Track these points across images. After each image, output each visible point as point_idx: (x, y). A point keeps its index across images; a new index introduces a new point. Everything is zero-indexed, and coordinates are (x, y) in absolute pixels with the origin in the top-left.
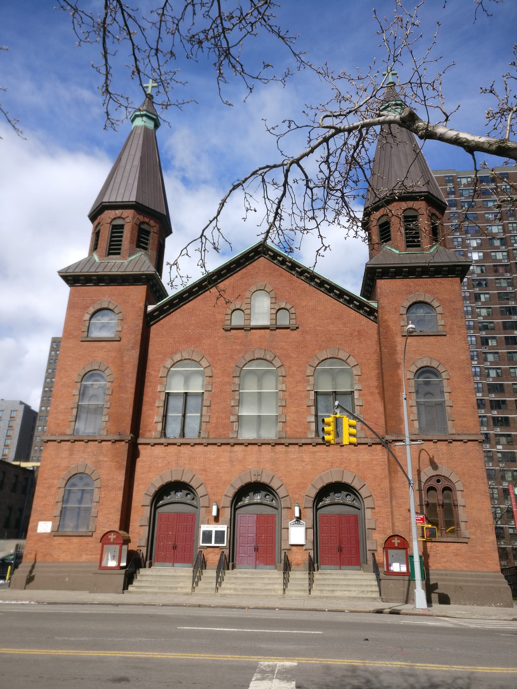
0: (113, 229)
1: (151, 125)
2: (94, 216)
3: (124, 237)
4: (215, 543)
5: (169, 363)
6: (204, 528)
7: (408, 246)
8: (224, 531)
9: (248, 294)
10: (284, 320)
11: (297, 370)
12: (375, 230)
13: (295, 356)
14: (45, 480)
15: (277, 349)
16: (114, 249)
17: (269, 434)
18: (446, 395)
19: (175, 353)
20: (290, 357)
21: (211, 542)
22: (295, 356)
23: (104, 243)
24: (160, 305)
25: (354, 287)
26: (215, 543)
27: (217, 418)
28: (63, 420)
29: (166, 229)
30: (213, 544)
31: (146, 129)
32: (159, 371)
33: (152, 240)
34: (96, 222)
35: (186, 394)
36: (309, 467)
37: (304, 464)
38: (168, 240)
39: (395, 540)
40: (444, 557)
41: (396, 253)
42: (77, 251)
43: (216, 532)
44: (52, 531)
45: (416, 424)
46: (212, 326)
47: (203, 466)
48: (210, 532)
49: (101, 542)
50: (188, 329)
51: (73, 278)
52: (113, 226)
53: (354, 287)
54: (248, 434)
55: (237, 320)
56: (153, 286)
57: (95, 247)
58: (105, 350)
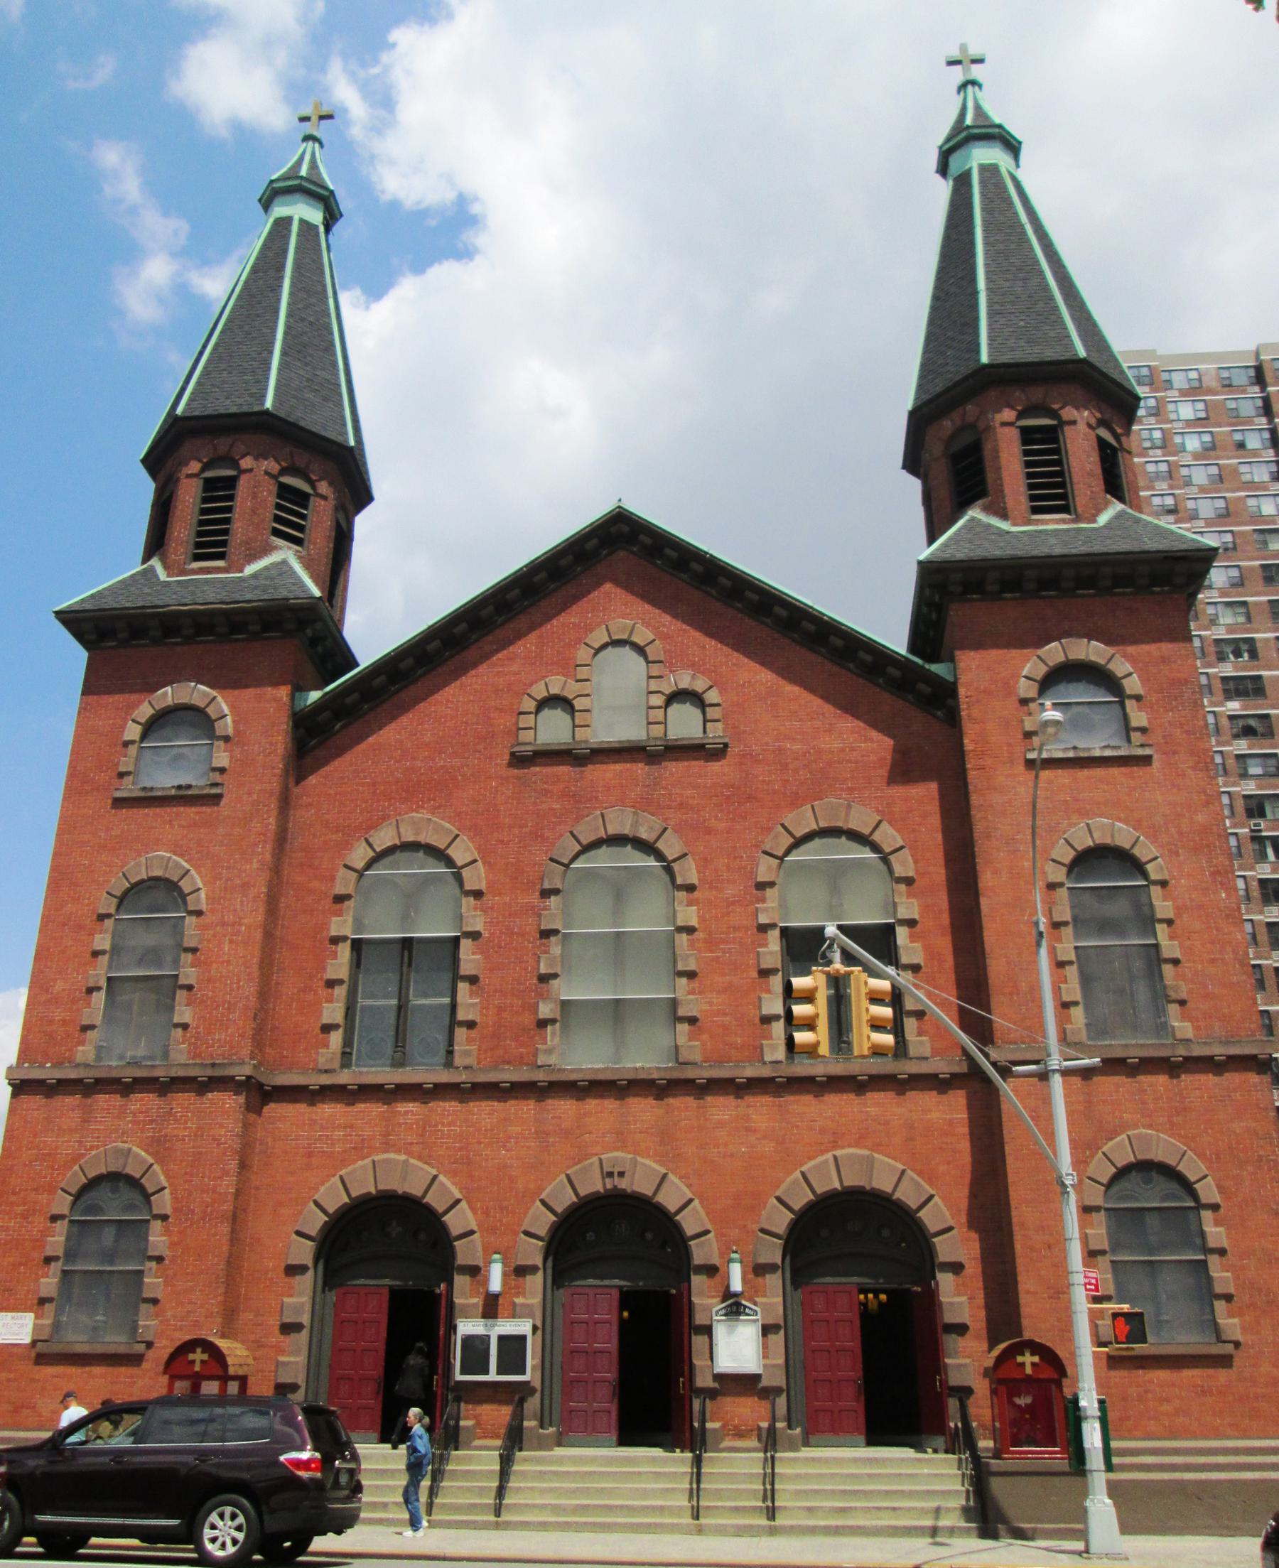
0: (205, 490)
1: (315, 216)
2: (160, 460)
3: (237, 510)
4: (499, 1373)
5: (360, 855)
6: (467, 1327)
7: (1036, 510)
8: (524, 1338)
9: (583, 654)
10: (684, 724)
11: (728, 866)
12: (941, 471)
13: (722, 826)
14: (14, 1193)
15: (669, 807)
16: (212, 543)
17: (645, 1056)
18: (1161, 929)
19: (374, 826)
20: (709, 831)
21: (487, 1373)
22: (722, 826)
23: (183, 529)
24: (343, 704)
25: (891, 629)
26: (499, 1373)
27: (500, 1010)
28: (64, 1023)
29: (357, 493)
30: (493, 1376)
31: (306, 226)
32: (333, 878)
33: (320, 515)
34: (162, 475)
35: (407, 943)
36: (768, 1147)
37: (752, 1139)
38: (364, 523)
39: (1023, 1355)
40: (1168, 1400)
41: (1004, 529)
42: (109, 553)
43: (502, 1339)
44: (34, 1343)
45: (1078, 1014)
46: (481, 747)
47: (460, 1149)
48: (485, 1339)
49: (165, 1372)
50: (414, 758)
51: (86, 624)
52: (207, 480)
53: (891, 629)
54: (585, 1056)
55: (552, 729)
56: (306, 632)
57: (156, 543)
58: (184, 823)
